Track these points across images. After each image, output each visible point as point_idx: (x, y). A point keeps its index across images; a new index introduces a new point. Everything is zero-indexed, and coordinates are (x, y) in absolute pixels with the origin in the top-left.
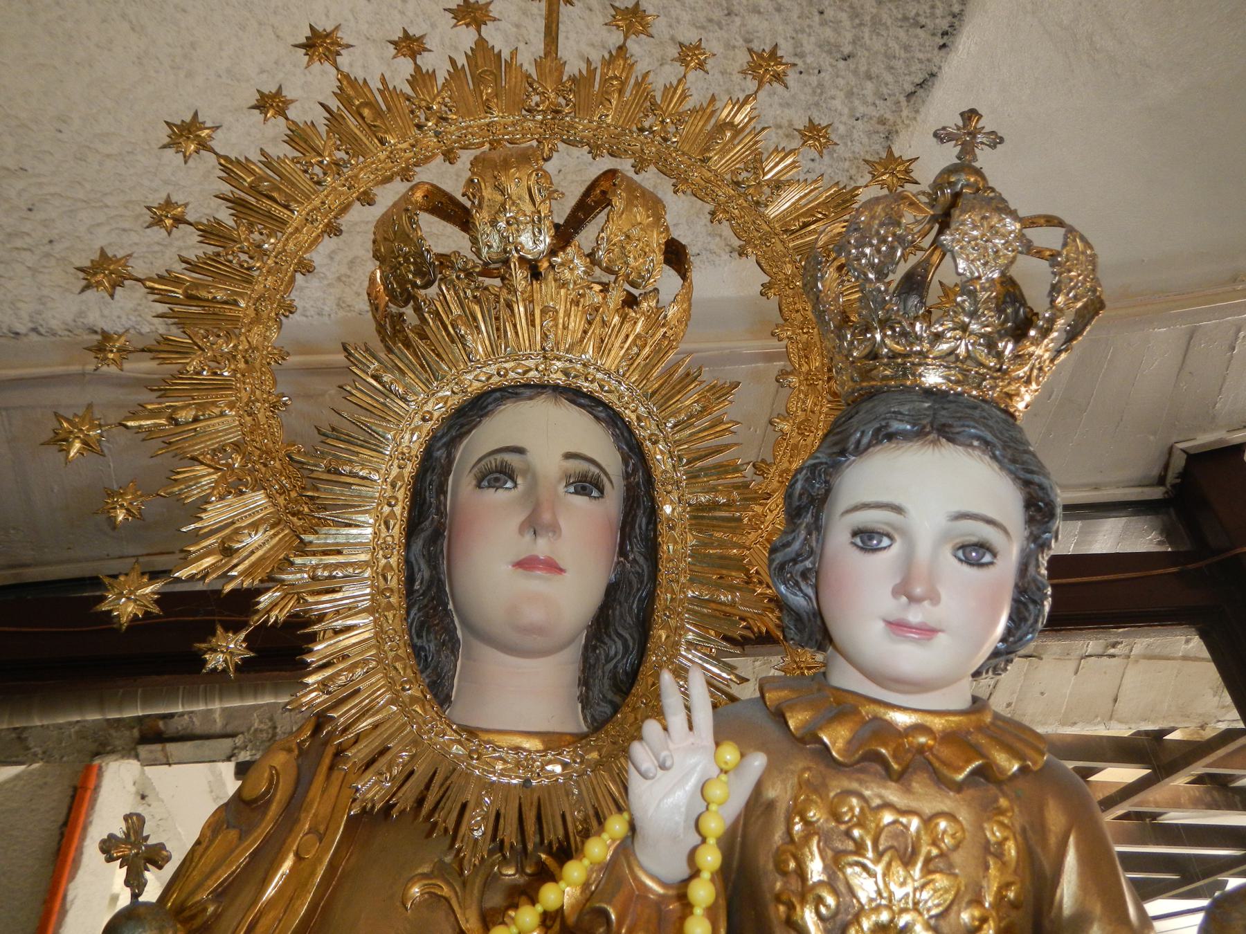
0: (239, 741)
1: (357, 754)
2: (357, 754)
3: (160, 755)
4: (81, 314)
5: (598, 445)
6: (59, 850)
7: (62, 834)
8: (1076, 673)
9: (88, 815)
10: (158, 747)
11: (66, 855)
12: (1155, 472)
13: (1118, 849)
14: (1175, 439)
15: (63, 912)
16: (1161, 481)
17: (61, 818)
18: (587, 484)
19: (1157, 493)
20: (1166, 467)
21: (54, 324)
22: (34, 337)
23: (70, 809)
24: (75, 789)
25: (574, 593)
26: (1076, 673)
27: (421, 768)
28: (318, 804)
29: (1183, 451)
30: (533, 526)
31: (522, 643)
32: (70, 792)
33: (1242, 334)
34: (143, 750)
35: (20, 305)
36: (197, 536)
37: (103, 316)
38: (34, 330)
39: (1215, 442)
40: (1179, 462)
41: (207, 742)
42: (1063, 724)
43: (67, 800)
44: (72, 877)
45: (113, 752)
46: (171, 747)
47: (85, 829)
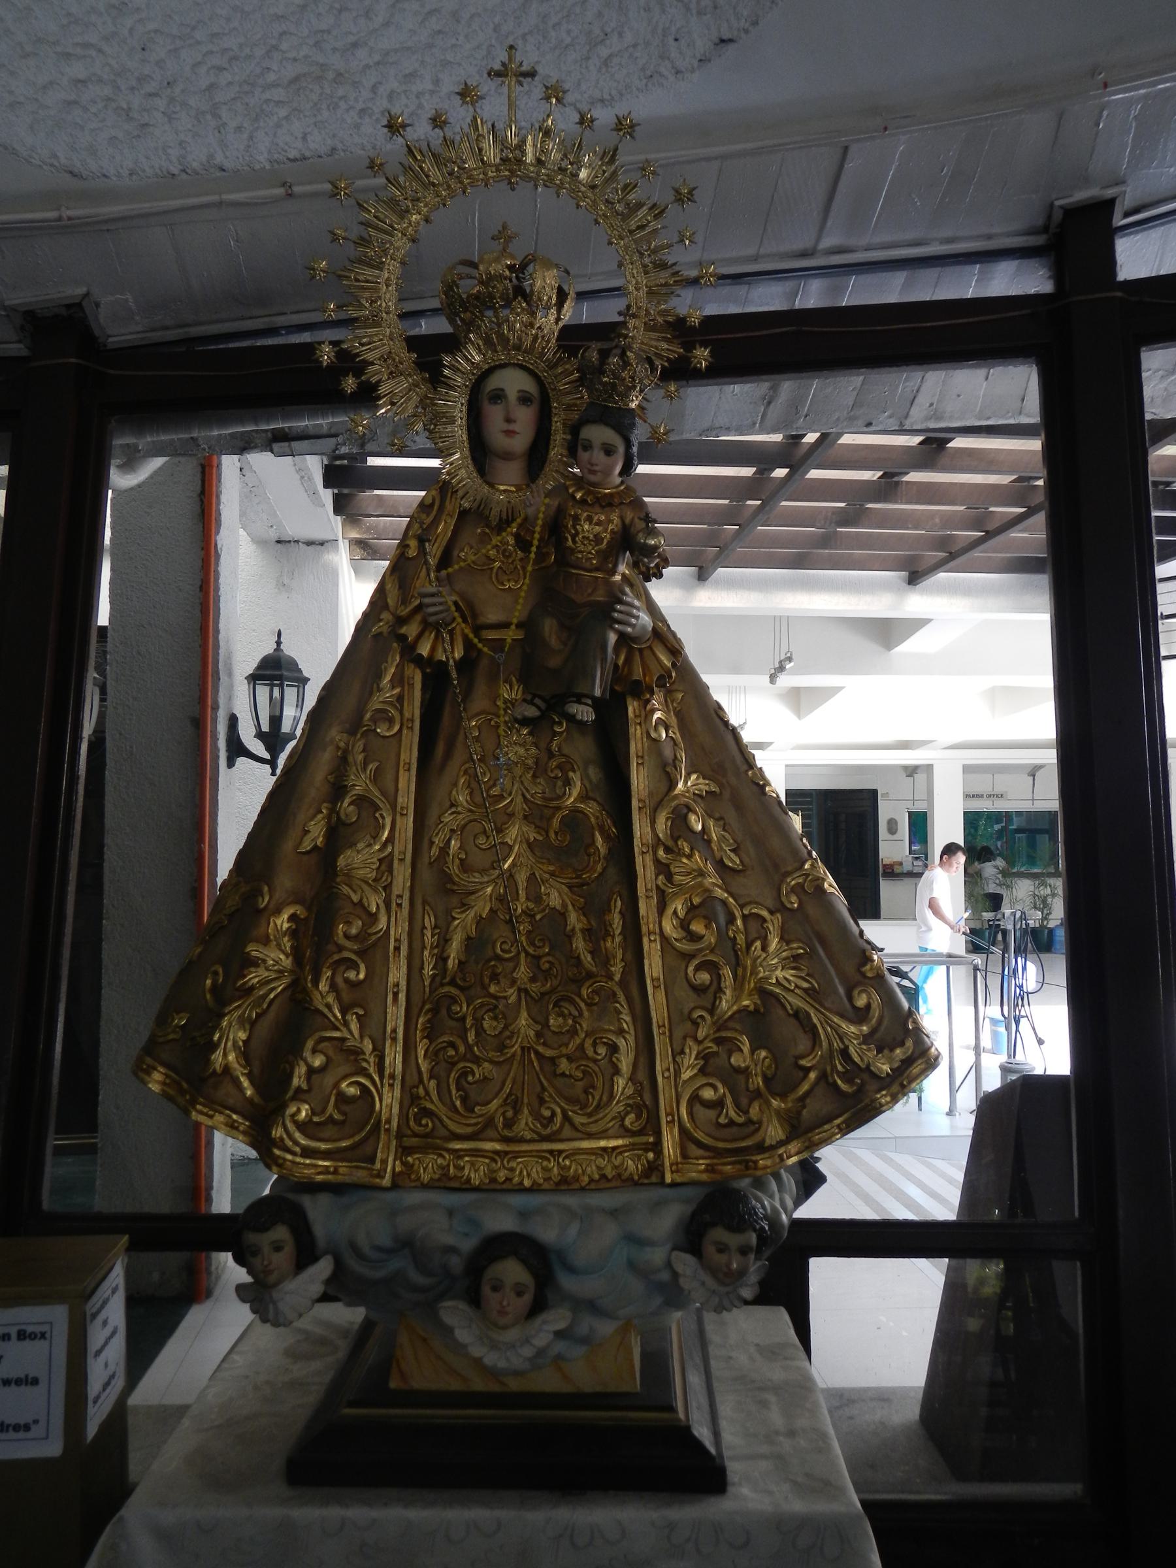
0: (340, 439)
1: (460, 493)
2: (460, 493)
3: (287, 450)
4: (211, 156)
5: (529, 385)
6: (203, 511)
7: (202, 500)
8: (987, 378)
9: (218, 487)
10: (286, 444)
11: (210, 515)
12: (1040, 222)
13: (1155, 513)
14: (1054, 196)
15: (218, 556)
16: (1045, 229)
17: (198, 489)
18: (525, 399)
19: (1039, 240)
20: (1049, 217)
21: (195, 165)
22: (184, 176)
23: (203, 481)
24: (203, 467)
25: (520, 442)
26: (987, 378)
27: (478, 498)
28: (449, 506)
29: (1061, 207)
30: (508, 420)
31: (507, 456)
32: (199, 469)
33: (1105, 113)
34: (276, 446)
35: (169, 151)
36: (379, 398)
37: (226, 157)
38: (184, 171)
39: (1092, 198)
40: (1058, 216)
41: (319, 441)
42: (980, 419)
43: (199, 476)
44: (218, 532)
45: (255, 447)
46: (295, 444)
47: (218, 497)
